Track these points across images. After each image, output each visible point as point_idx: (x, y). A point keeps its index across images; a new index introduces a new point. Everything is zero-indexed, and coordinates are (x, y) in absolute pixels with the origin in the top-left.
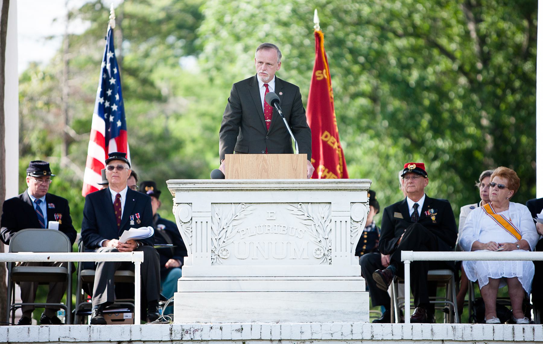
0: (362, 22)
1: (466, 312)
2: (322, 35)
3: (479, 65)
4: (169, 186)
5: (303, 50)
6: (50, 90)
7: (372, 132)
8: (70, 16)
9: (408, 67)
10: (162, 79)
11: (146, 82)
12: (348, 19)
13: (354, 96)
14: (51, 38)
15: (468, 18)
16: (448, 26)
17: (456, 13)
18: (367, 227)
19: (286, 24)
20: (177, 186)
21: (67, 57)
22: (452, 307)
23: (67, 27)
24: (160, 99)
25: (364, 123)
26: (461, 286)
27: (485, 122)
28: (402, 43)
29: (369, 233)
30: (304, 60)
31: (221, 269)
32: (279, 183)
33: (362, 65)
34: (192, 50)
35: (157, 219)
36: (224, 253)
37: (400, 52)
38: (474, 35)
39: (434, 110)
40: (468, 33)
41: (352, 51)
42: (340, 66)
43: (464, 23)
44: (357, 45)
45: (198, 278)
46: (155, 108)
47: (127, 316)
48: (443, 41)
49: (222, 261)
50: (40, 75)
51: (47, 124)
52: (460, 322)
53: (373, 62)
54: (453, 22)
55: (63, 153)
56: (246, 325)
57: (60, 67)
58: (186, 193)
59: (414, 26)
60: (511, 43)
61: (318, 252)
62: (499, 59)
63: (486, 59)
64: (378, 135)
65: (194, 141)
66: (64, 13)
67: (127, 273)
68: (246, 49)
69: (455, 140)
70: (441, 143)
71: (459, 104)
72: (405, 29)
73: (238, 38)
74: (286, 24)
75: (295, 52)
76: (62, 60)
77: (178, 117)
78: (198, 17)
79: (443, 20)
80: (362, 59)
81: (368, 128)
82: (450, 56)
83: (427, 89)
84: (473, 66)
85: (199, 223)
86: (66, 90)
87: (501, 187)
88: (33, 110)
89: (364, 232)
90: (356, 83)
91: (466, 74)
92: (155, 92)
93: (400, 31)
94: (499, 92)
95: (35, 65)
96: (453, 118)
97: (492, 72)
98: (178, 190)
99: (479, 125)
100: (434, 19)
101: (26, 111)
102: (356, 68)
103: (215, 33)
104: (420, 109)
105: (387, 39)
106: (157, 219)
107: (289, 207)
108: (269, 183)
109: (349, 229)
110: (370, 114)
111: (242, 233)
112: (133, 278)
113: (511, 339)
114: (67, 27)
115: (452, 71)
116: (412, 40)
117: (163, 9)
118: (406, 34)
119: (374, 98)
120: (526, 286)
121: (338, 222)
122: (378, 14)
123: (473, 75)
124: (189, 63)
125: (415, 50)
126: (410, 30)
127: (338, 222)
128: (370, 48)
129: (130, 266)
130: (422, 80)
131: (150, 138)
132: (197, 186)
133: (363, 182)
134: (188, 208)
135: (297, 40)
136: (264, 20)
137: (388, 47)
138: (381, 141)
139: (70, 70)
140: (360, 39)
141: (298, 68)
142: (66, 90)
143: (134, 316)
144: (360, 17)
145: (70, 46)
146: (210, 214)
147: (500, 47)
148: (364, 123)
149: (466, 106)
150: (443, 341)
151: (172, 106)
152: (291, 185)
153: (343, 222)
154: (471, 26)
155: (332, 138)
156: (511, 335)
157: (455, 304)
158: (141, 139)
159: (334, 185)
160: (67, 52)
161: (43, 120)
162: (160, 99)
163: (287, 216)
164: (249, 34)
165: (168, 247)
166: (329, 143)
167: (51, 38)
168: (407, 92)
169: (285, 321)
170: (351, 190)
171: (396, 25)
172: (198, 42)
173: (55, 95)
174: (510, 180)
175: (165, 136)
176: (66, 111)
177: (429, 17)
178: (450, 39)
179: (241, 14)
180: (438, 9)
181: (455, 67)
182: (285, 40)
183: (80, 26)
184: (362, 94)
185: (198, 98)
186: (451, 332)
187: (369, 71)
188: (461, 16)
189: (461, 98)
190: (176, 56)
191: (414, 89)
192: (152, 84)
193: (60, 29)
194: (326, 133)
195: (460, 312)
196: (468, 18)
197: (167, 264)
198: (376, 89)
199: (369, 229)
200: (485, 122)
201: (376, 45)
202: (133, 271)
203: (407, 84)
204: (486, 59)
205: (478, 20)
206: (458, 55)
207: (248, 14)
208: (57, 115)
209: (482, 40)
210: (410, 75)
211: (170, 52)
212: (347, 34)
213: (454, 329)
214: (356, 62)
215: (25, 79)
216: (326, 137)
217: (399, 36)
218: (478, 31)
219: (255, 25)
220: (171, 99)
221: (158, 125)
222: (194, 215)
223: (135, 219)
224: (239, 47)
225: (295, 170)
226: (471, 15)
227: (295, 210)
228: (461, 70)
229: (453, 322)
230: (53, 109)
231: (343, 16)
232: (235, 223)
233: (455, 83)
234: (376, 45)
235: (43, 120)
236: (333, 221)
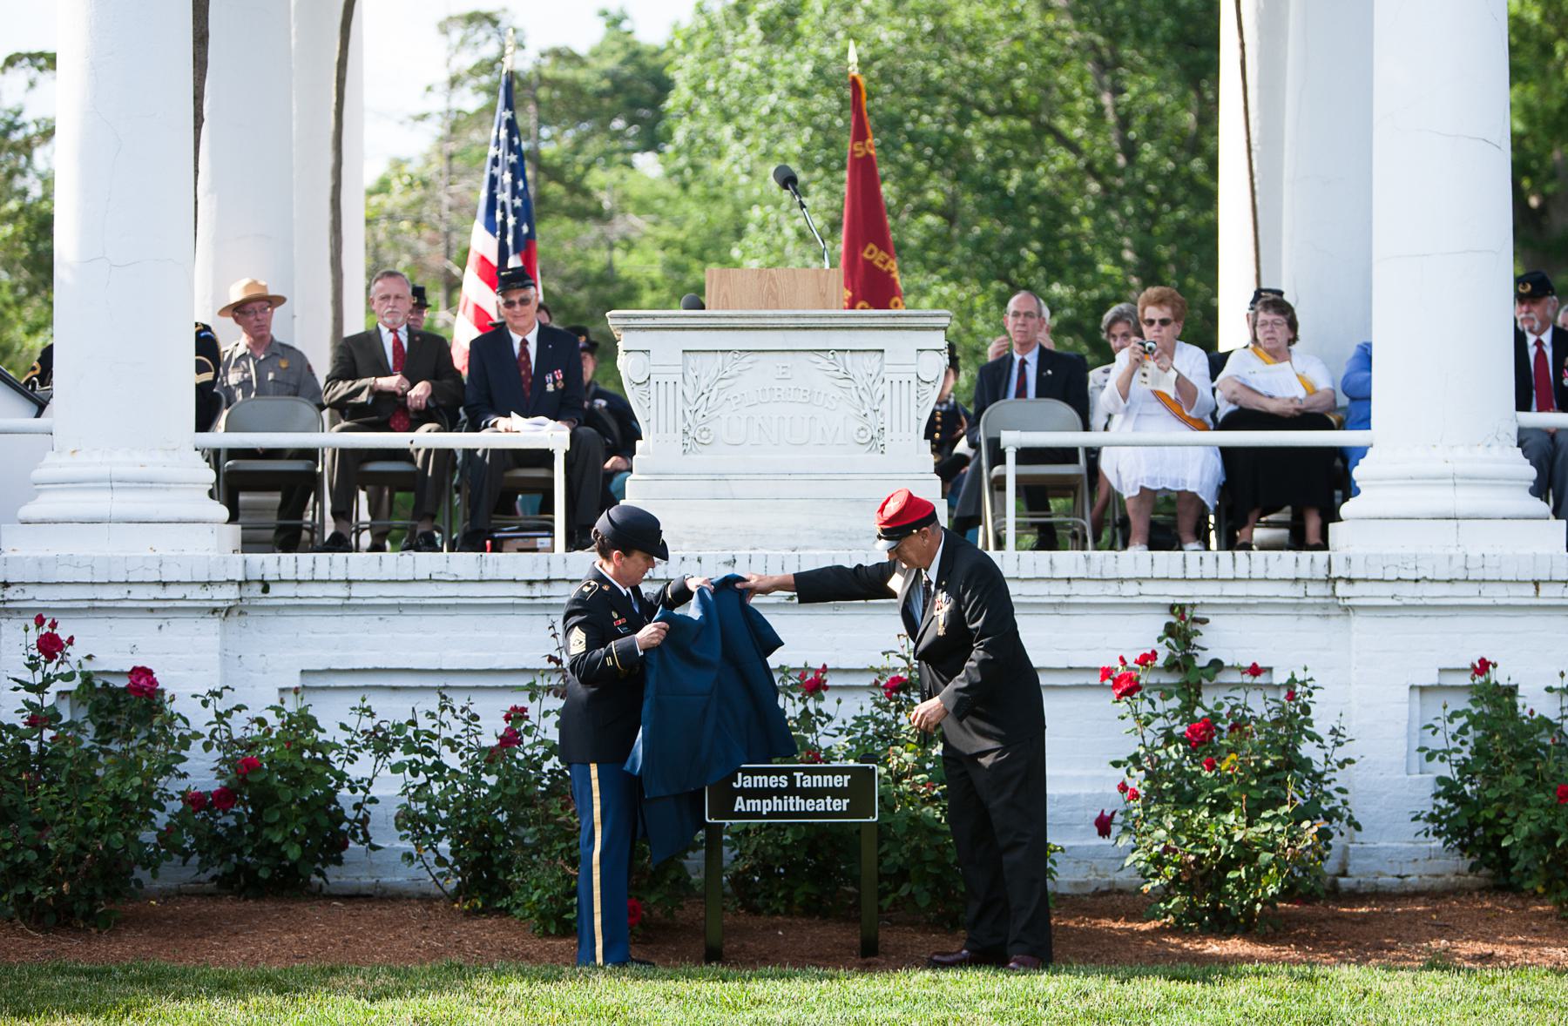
0: (931, 92)
1: (1106, 536)
2: (862, 81)
3: (1121, 161)
4: (610, 322)
5: (832, 135)
6: (422, 201)
7: (945, 271)
8: (454, 82)
9: (1003, 163)
10: (602, 188)
11: (576, 187)
12: (905, 83)
13: (918, 211)
14: (423, 117)
15: (1102, 86)
16: (1071, 99)
17: (1081, 78)
18: (939, 403)
19: (805, 94)
20: (625, 322)
21: (452, 147)
22: (1084, 528)
23: (449, 100)
24: (600, 216)
25: (932, 255)
26: (1100, 499)
27: (1128, 255)
28: (997, 125)
29: (944, 414)
30: (832, 152)
31: (702, 460)
32: (797, 316)
33: (931, 159)
34: (653, 141)
35: (592, 389)
36: (704, 434)
37: (994, 137)
38: (1109, 112)
39: (1048, 236)
40: (1100, 109)
41: (913, 138)
42: (895, 162)
43: (1094, 95)
44: (921, 128)
45: (659, 475)
46: (592, 230)
47: (543, 542)
48: (1062, 124)
49: (700, 447)
50: (406, 179)
51: (417, 256)
52: (1097, 548)
53: (950, 156)
54: (1077, 91)
55: (443, 305)
56: (742, 555)
57: (439, 164)
58: (639, 333)
59: (1015, 99)
60: (1167, 125)
61: (862, 433)
62: (1148, 152)
63: (1130, 150)
64: (956, 277)
65: (654, 288)
66: (445, 76)
67: (540, 473)
68: (740, 134)
69: (1080, 286)
70: (1057, 289)
71: (1087, 224)
72: (1000, 102)
73: (727, 117)
74: (805, 94)
75: (819, 138)
76: (440, 152)
77: (630, 246)
78: (664, 86)
79: (1062, 88)
80: (929, 151)
81: (942, 264)
82: (1073, 146)
83: (1035, 199)
84: (1110, 163)
85: (662, 384)
86: (447, 200)
87: (1164, 322)
88: (392, 235)
89: (934, 412)
90: (918, 191)
91: (1098, 177)
92: (592, 206)
93: (991, 106)
94: (1150, 205)
95: (398, 164)
96: (1076, 248)
97: (1140, 175)
98: (625, 329)
99: (1119, 261)
100: (1047, 88)
101: (381, 236)
102: (921, 167)
103: (690, 110)
104: (1024, 232)
105: (971, 119)
106: (592, 389)
107: (814, 357)
108: (780, 317)
109: (914, 395)
110: (945, 241)
111: (733, 402)
112: (551, 481)
113: (1181, 575)
114: (449, 100)
115: (1074, 171)
116: (1012, 121)
117: (606, 75)
118: (1001, 112)
119: (949, 214)
120: (1210, 499)
121: (896, 384)
122: (956, 78)
123: (1110, 179)
124: (648, 164)
125: (1016, 137)
126: (1008, 103)
127: (896, 384)
128: (942, 133)
129: (543, 458)
130: (1029, 183)
131: (583, 280)
132: (658, 321)
133: (938, 316)
134: (648, 363)
135: (822, 120)
136: (770, 88)
137: (969, 133)
138: (961, 285)
139: (453, 163)
140: (926, 119)
141: (824, 165)
142: (447, 200)
143: (553, 543)
144: (927, 82)
145: (453, 129)
146: (680, 369)
147: (1151, 133)
148: (932, 255)
149: (1098, 230)
150: (1069, 579)
151: (619, 226)
152: (817, 321)
153: (905, 384)
154: (1106, 99)
155: (883, 254)
156: (1181, 569)
157: (1087, 524)
158: (567, 280)
159: (889, 321)
160: (449, 140)
161: (409, 249)
162: (600, 216)
163: (812, 372)
164: (744, 110)
165: (610, 430)
166: (876, 263)
167: (423, 117)
168: (1006, 207)
169: (807, 548)
170: (917, 329)
171: (985, 95)
172: (661, 128)
173: (426, 210)
174: (1173, 307)
175: (607, 276)
176: (447, 235)
177: (1039, 84)
178: (1070, 115)
179: (732, 76)
180: (1053, 70)
181: (1082, 163)
182: (802, 119)
183: (470, 101)
184: (929, 208)
185: (659, 218)
186: (1082, 564)
187: (940, 169)
188: (1090, 82)
189: (1094, 215)
190: (626, 151)
191: (1013, 200)
192: (587, 193)
193: (437, 103)
194: (871, 246)
195: (1097, 538)
196: (1102, 86)
197: (608, 465)
198: (954, 199)
199: (944, 407)
200: (1128, 255)
201: (951, 128)
202: (552, 468)
203: (1003, 190)
204: (1130, 150)
205: (1117, 91)
206: (1085, 145)
207: (743, 77)
208: (433, 242)
209: (1124, 123)
210: (1008, 178)
211: (617, 144)
212: (907, 110)
213: (1087, 559)
214: (919, 156)
215: (383, 187)
216: (871, 252)
217: (992, 115)
218: (1116, 106)
219: (756, 94)
220: (618, 218)
221: (598, 260)
222: (653, 370)
223: (555, 381)
224: (728, 131)
225: (823, 295)
226: (1107, 79)
227: (824, 362)
228: (1090, 168)
229: (1084, 548)
230: (427, 233)
231: (897, 79)
232: (722, 384)
233: (1081, 189)
234: (951, 128)
235: (409, 249)
236: (887, 381)
